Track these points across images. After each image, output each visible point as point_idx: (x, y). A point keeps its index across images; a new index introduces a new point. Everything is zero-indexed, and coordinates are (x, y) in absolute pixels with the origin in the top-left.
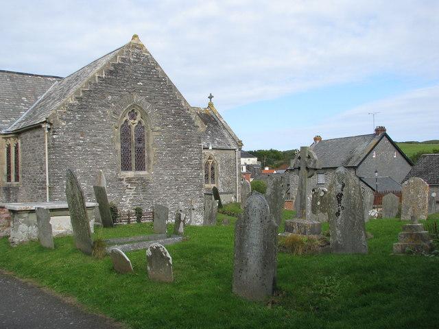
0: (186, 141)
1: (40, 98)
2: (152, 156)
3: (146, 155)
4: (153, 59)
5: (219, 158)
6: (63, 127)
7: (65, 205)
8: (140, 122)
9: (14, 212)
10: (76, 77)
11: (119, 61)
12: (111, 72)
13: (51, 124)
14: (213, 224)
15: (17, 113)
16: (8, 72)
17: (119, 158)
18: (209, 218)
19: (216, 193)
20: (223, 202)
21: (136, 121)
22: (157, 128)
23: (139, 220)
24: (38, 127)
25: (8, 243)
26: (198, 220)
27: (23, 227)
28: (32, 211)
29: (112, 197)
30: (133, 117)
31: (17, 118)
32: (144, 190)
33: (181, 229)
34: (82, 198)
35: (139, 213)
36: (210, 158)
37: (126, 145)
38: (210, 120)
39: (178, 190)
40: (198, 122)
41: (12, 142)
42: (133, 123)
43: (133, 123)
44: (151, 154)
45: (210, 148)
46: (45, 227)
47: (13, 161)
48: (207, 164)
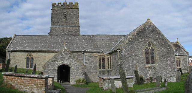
0: (169, 53)
1: (118, 42)
2: (157, 59)
3: (155, 58)
4: (155, 26)
5: (181, 58)
6: (124, 50)
7: (120, 77)
8: (152, 48)
9: (104, 79)
10: (129, 35)
11: (143, 28)
12: (141, 32)
13: (120, 50)
14: (179, 81)
15: (111, 47)
16: (109, 35)
17: (145, 60)
18: (178, 79)
19: (180, 70)
20: (183, 73)
21: (151, 47)
22: (158, 49)
23: (151, 81)
24: (116, 51)
25: (102, 89)
26: (174, 80)
27: (107, 84)
28: (109, 79)
29: (140, 74)
30: (149, 46)
31: (111, 49)
32: (154, 71)
33: (166, 85)
34: (125, 75)
35: (151, 79)
36: (178, 59)
37: (147, 56)
38: (178, 46)
39: (167, 70)
40: (173, 47)
41: (109, 56)
42: (149, 48)
43: (149, 48)
44: (156, 58)
45: (178, 55)
46: (113, 85)
47: (109, 62)
48: (177, 61)
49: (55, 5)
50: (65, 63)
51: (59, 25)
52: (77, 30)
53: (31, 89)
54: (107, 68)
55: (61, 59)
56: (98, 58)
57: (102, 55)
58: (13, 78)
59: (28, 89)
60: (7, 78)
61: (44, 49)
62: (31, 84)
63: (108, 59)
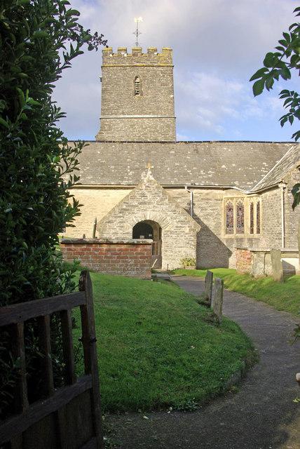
49: (111, 55)
50: (150, 215)
51: (123, 113)
52: (168, 126)
53: (124, 270)
54: (249, 232)
55: (142, 207)
56: (223, 205)
57: (235, 196)
58: (120, 250)
59: (118, 270)
60: (70, 250)
61: (91, 179)
62: (123, 258)
63: (252, 209)
